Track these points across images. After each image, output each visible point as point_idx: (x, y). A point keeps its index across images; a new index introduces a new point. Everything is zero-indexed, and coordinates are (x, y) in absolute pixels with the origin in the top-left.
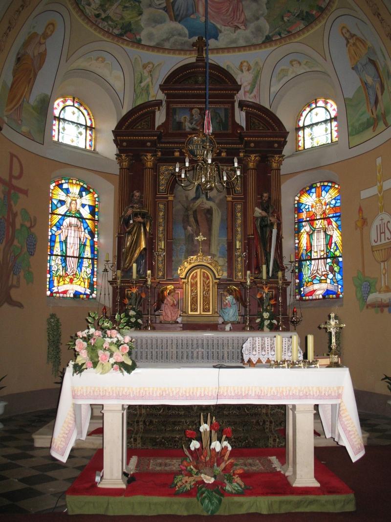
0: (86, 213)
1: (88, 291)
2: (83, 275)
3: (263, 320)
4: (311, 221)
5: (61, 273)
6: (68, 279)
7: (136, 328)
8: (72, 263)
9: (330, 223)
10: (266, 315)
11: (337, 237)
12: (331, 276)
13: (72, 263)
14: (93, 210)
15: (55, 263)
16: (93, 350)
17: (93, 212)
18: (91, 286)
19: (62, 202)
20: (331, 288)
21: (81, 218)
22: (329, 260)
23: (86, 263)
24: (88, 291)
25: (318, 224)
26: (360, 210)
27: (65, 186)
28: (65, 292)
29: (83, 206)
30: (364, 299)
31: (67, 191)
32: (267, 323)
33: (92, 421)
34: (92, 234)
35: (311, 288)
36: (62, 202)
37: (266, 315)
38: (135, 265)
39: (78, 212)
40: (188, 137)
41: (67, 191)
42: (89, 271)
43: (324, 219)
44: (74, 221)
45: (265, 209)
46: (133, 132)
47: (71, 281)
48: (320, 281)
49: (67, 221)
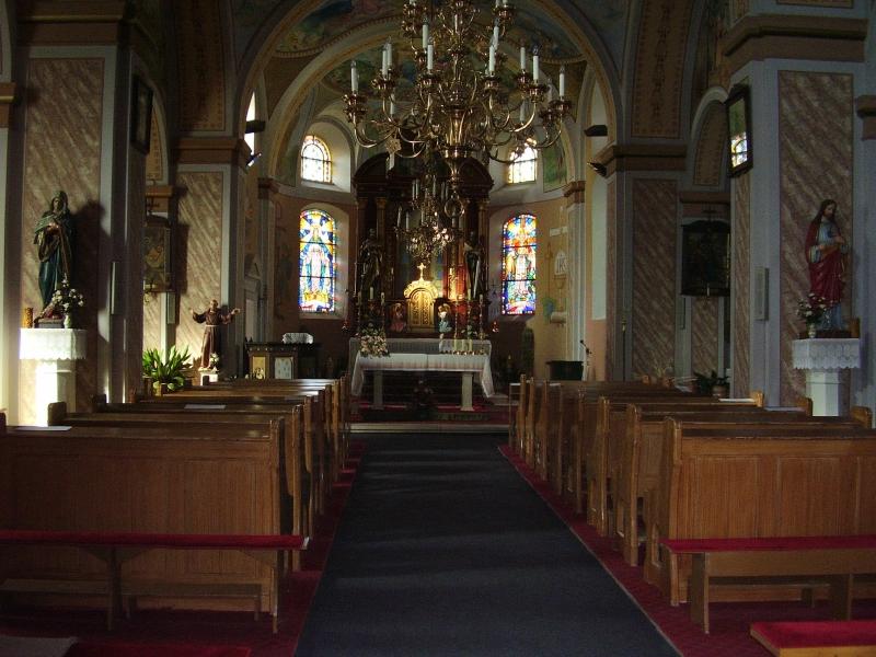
0: (325, 239)
1: (328, 306)
2: (324, 292)
3: (466, 331)
4: (516, 247)
5: (307, 291)
6: (312, 296)
7: (179, 366)
8: (316, 281)
9: (530, 251)
10: (469, 327)
11: (533, 259)
12: (529, 295)
13: (316, 281)
14: (331, 235)
15: (303, 282)
16: (370, 346)
17: (331, 238)
18: (330, 301)
19: (307, 232)
20: (529, 305)
21: (322, 244)
22: (528, 282)
23: (326, 281)
24: (328, 306)
25: (522, 251)
26: (549, 245)
27: (309, 217)
28: (310, 307)
29: (323, 233)
30: (548, 316)
31: (311, 222)
32: (469, 333)
33: (378, 380)
34: (330, 256)
35: (514, 305)
36: (307, 232)
37: (469, 327)
38: (372, 289)
39: (320, 239)
40: (419, 270)
41: (311, 222)
42: (329, 288)
43: (526, 246)
44: (317, 246)
45: (473, 245)
46: (366, 174)
47: (315, 297)
48: (522, 299)
49: (312, 246)
